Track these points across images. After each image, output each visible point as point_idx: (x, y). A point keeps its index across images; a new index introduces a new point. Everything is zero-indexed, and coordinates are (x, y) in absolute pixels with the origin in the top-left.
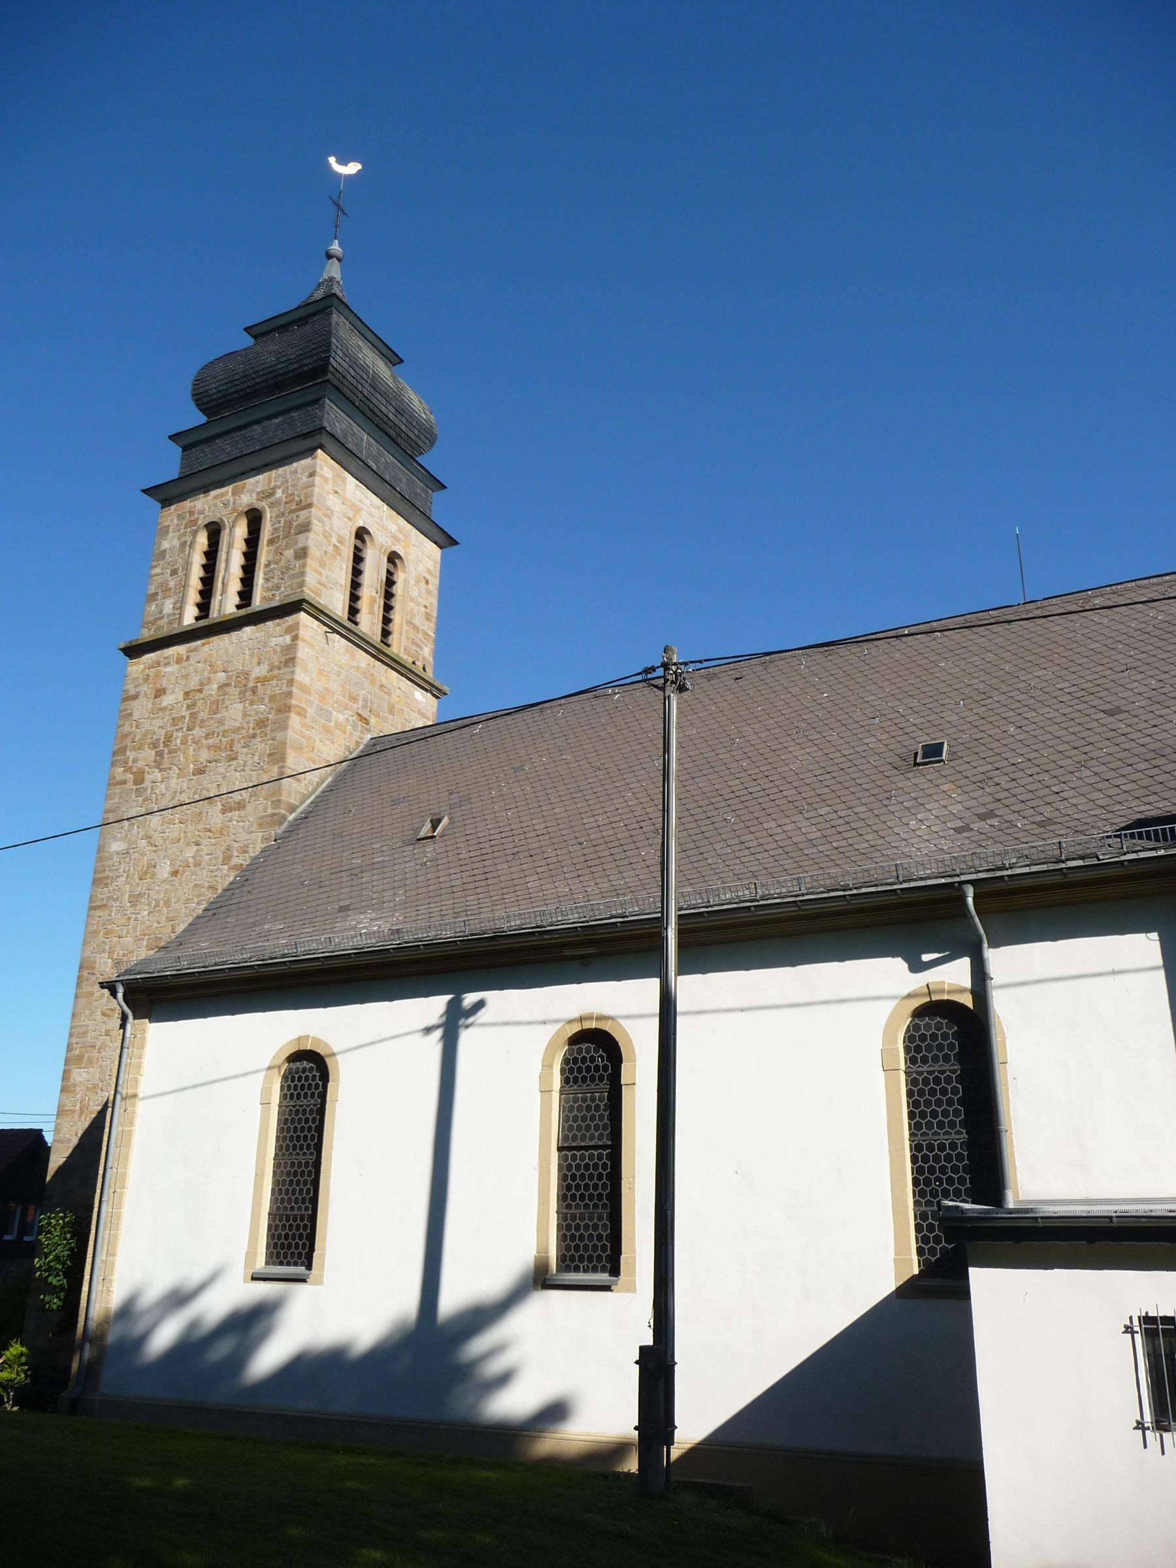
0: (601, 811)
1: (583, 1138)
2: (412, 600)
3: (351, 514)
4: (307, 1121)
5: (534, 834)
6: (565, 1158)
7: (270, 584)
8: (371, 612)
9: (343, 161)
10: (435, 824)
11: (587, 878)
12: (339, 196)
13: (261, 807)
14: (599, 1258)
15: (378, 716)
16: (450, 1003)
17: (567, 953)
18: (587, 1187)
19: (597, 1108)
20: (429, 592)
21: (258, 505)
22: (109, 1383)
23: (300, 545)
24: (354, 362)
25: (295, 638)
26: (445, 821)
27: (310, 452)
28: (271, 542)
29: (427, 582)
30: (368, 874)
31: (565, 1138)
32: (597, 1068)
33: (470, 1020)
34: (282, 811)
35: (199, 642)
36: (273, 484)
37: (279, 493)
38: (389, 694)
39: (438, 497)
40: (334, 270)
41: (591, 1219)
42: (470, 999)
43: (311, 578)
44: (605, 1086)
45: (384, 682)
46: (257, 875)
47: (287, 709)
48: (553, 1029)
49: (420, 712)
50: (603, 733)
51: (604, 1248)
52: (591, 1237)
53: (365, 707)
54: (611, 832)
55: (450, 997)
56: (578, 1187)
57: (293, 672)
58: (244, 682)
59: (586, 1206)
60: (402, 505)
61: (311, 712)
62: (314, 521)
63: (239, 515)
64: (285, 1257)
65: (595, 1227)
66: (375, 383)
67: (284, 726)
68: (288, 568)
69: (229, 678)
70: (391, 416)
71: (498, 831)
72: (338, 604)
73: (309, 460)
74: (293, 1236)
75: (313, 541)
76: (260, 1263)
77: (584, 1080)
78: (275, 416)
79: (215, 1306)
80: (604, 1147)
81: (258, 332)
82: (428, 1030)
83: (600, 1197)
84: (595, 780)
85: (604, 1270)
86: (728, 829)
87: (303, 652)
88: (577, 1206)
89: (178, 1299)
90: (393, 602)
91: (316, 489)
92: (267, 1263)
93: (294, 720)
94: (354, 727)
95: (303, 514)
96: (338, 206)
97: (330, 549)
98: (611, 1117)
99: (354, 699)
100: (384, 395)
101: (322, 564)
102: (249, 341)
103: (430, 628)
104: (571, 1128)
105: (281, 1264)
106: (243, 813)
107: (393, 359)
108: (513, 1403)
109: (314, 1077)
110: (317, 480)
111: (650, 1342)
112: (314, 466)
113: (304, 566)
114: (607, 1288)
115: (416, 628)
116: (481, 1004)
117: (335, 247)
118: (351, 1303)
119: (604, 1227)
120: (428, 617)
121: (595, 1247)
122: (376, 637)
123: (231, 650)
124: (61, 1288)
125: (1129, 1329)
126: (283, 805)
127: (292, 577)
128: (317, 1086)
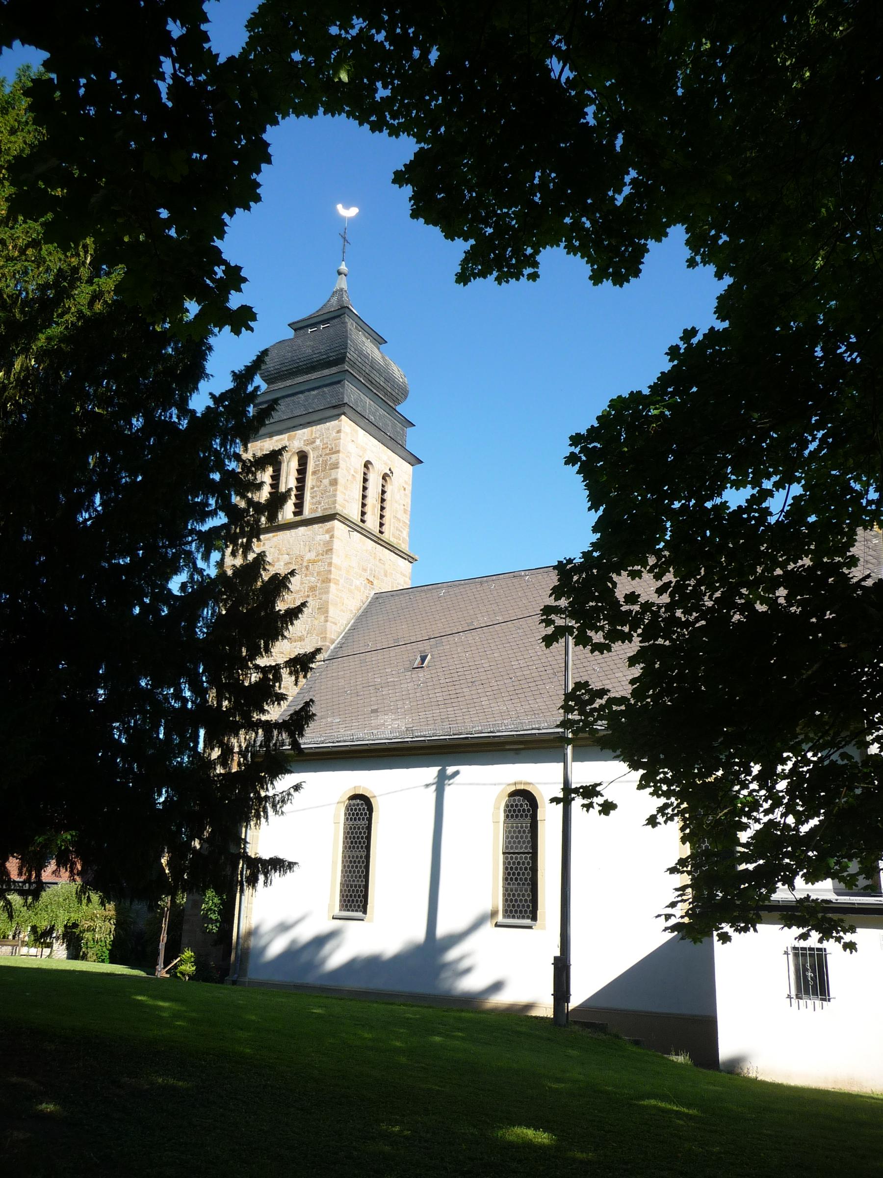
0: (522, 657)
1: (517, 848)
2: (396, 502)
3: (361, 454)
4: (360, 833)
5: (482, 670)
6: (507, 858)
7: (314, 500)
8: (373, 514)
9: (347, 206)
10: (423, 659)
11: (516, 701)
12: (345, 235)
13: (314, 641)
14: (526, 912)
15: (378, 579)
16: (439, 771)
17: (508, 747)
18: (519, 874)
19: (524, 832)
20: (405, 495)
21: (306, 449)
22: (253, 974)
23: (333, 477)
24: (361, 353)
25: (332, 537)
26: (429, 657)
27: (337, 416)
28: (314, 473)
29: (405, 489)
30: (386, 689)
31: (507, 847)
32: (524, 810)
33: (451, 781)
34: (328, 644)
35: (271, 535)
36: (314, 436)
37: (318, 442)
38: (384, 564)
39: (410, 430)
40: (343, 283)
41: (521, 891)
42: (450, 770)
43: (340, 498)
44: (528, 820)
45: (382, 558)
46: (317, 685)
47: (328, 580)
48: (502, 787)
49: (402, 574)
50: (520, 603)
51: (528, 906)
52: (521, 900)
53: (371, 574)
54: (528, 672)
55: (440, 768)
56: (514, 874)
57: (331, 558)
58: (300, 562)
59: (519, 884)
60: (391, 443)
61: (341, 581)
62: (341, 462)
63: (293, 454)
64: (351, 906)
65: (523, 895)
66: (373, 365)
67: (327, 592)
68: (325, 491)
69: (291, 559)
70: (382, 383)
71: (461, 666)
72: (356, 516)
73: (336, 422)
74: (355, 896)
75: (341, 475)
76: (336, 911)
77: (517, 816)
78: (313, 389)
79: (305, 933)
80: (528, 853)
81: (298, 327)
82: (427, 786)
83: (526, 879)
84: (517, 635)
85: (528, 918)
86: (595, 676)
87: (337, 545)
88: (514, 884)
89: (284, 928)
90: (385, 504)
91: (342, 441)
92: (340, 910)
93: (333, 587)
94: (365, 588)
95: (334, 456)
96: (345, 238)
97: (350, 478)
98: (531, 837)
99: (365, 570)
100: (378, 371)
101: (346, 488)
102: (290, 334)
103: (406, 518)
104: (510, 842)
105: (348, 910)
106: (302, 643)
107: (379, 341)
108: (471, 983)
109: (364, 809)
110: (342, 434)
111: (558, 954)
112: (340, 426)
113: (336, 490)
114: (530, 927)
115: (399, 520)
116: (457, 773)
117: (343, 267)
118: (385, 932)
119: (528, 895)
120: (405, 511)
121: (523, 906)
122: (376, 530)
123: (291, 541)
124: (217, 921)
125: (786, 953)
126: (328, 640)
127: (330, 497)
128: (366, 814)
